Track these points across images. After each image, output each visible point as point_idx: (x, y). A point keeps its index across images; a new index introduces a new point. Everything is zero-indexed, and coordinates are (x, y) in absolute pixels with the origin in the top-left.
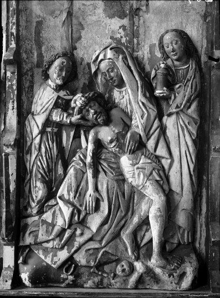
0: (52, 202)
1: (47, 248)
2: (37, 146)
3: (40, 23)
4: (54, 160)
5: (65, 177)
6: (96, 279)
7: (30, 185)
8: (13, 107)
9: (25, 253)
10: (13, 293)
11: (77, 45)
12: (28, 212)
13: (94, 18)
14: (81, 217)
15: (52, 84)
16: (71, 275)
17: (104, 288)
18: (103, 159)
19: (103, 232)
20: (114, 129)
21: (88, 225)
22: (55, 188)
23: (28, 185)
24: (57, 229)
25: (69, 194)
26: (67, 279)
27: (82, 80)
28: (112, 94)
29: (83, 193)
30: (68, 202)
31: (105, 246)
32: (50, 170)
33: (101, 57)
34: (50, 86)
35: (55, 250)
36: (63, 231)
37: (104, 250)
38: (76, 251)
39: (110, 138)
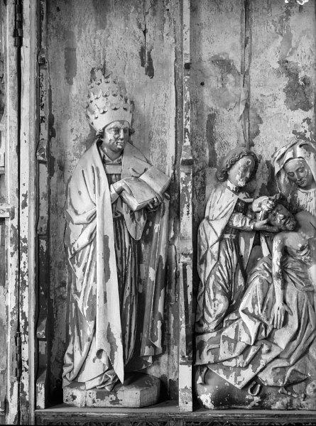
0: (233, 316)
1: (228, 367)
2: (216, 255)
3: (212, 117)
4: (234, 271)
5: (246, 289)
6: (286, 400)
7: (204, 299)
8: (188, 212)
9: (203, 373)
10: (195, 415)
11: (255, 141)
12: (204, 327)
13: (274, 111)
14: (268, 332)
15: (232, 186)
16: (257, 395)
17: (294, 409)
18: (290, 269)
19: (291, 348)
20: (304, 235)
21: (275, 341)
22: (234, 302)
23: (202, 299)
24: (240, 346)
25: (254, 308)
26: (253, 400)
27: (262, 180)
28: (296, 195)
29: (270, 305)
30: (252, 316)
31: (293, 365)
32: (230, 282)
33: (289, 155)
34: (229, 188)
35: (238, 369)
36: (248, 347)
37: (292, 368)
38: (261, 370)
39: (300, 245)
